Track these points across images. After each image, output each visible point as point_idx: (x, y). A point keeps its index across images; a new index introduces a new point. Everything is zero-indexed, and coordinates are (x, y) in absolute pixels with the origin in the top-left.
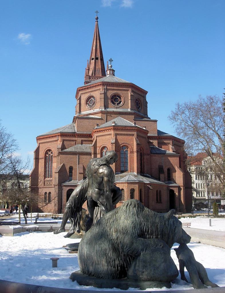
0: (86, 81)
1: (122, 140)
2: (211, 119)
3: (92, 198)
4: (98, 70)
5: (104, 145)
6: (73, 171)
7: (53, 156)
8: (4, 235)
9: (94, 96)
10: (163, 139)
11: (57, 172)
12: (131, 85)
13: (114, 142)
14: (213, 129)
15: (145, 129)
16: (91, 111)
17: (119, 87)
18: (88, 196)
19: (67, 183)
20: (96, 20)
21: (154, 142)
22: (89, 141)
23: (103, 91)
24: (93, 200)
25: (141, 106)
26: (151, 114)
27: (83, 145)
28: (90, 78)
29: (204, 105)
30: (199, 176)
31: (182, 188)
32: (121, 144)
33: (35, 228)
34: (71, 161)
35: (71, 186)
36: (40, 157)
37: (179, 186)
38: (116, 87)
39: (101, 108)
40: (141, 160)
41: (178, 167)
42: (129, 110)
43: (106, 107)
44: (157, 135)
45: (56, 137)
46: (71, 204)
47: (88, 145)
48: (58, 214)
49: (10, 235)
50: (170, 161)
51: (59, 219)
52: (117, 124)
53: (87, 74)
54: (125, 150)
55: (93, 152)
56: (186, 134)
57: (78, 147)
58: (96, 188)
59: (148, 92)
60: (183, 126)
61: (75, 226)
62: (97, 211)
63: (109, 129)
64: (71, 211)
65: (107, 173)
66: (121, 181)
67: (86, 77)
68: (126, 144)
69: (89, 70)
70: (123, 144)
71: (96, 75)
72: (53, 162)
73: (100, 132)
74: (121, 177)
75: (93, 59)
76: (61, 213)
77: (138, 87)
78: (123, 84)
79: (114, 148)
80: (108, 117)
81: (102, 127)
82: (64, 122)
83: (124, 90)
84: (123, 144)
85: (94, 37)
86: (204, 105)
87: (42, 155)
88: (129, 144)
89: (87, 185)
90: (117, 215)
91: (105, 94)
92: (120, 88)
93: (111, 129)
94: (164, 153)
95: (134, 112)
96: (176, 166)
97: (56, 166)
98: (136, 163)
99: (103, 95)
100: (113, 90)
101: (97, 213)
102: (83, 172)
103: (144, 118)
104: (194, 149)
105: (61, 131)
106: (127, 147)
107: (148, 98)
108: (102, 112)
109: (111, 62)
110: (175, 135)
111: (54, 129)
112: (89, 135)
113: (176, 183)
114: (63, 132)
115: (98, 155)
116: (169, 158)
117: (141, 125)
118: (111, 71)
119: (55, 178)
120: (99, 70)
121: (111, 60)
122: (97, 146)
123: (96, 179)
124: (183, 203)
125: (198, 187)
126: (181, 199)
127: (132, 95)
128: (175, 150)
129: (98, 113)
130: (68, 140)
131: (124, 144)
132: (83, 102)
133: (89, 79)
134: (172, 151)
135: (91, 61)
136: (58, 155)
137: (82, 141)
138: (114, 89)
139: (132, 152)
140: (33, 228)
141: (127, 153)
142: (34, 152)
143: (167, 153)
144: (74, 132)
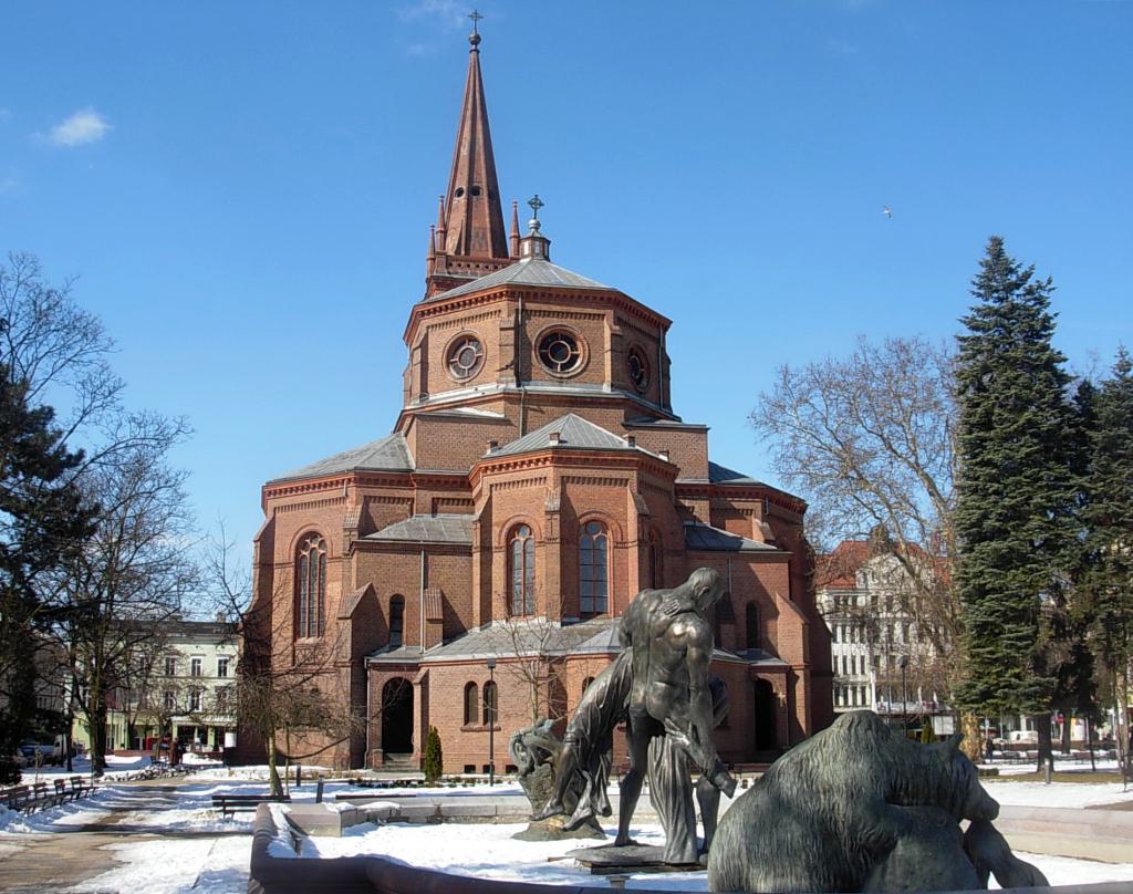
0: (435, 274)
1: (586, 499)
2: (904, 424)
3: (645, 711)
4: (481, 235)
5: (521, 519)
6: (405, 612)
7: (329, 555)
8: (312, 832)
9: (478, 334)
10: (730, 495)
11: (349, 615)
12: (613, 297)
13: (557, 509)
14: (912, 460)
15: (664, 458)
16: (463, 392)
17: (568, 305)
18: (632, 705)
19: (384, 655)
20: (474, 47)
21: (696, 506)
22: (461, 502)
23: (512, 318)
24: (649, 716)
25: (649, 373)
26: (684, 403)
27: (440, 516)
28: (451, 265)
29: (878, 373)
30: (844, 627)
31: (800, 673)
32: (580, 517)
33: (391, 809)
34: (401, 576)
35: (398, 667)
36: (277, 559)
37: (791, 667)
38: (558, 304)
39: (502, 383)
40: (652, 568)
41: (783, 598)
42: (606, 389)
43: (522, 377)
44: (708, 483)
45: (340, 486)
46: (582, 728)
47: (458, 517)
48: (354, 771)
49: (329, 831)
50: (756, 578)
51: (379, 787)
52: (565, 442)
53: (437, 250)
54: (595, 537)
55: (476, 542)
56: (814, 480)
57: (420, 523)
58: (660, 681)
59: (671, 322)
60: (803, 449)
61: (596, 795)
62: (659, 750)
63: (538, 460)
64: (583, 750)
65: (699, 635)
66: (584, 649)
67: (434, 259)
68: (598, 515)
69: (445, 233)
70: (587, 514)
71: (473, 254)
72: (328, 577)
73: (503, 470)
74: (581, 635)
75: (460, 192)
76: (361, 767)
77: (647, 309)
78: (584, 295)
79: (558, 528)
80: (530, 413)
81: (510, 452)
82: (361, 424)
83: (586, 314)
84: (589, 516)
85: (466, 109)
86: (878, 373)
87: (283, 550)
88: (609, 516)
89: (630, 670)
90: (824, 750)
91: (519, 329)
92: (573, 310)
93: (546, 459)
94: (733, 548)
95: (623, 397)
96: (778, 596)
97: (339, 592)
98: (637, 582)
99: (512, 332)
100: (549, 316)
101: (658, 755)
102: (441, 617)
103: (660, 419)
104: (834, 527)
105: (357, 463)
106: (604, 527)
107: (673, 343)
108: (507, 397)
109: (536, 209)
110: (775, 482)
111: (325, 457)
112: (459, 480)
113: (778, 657)
114: (364, 469)
115: (494, 555)
116: (753, 566)
117: (652, 444)
118: (537, 243)
119: (339, 637)
120: (484, 234)
121: (536, 204)
122: (494, 521)
123: (664, 655)
124: (803, 726)
125: (849, 670)
126: (798, 715)
127: (617, 335)
128: (774, 535)
129: (495, 400)
130: (385, 498)
131: (594, 515)
132: (436, 355)
133: (447, 268)
134: (763, 539)
135: (451, 199)
136: (347, 552)
137: (435, 501)
138: (549, 312)
139: (621, 544)
140: (383, 811)
141: (601, 547)
142: (255, 541)
143: (743, 546)
144: (404, 467)
